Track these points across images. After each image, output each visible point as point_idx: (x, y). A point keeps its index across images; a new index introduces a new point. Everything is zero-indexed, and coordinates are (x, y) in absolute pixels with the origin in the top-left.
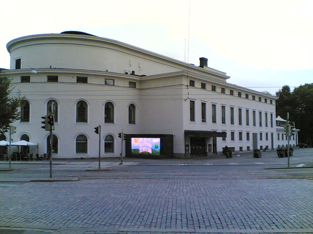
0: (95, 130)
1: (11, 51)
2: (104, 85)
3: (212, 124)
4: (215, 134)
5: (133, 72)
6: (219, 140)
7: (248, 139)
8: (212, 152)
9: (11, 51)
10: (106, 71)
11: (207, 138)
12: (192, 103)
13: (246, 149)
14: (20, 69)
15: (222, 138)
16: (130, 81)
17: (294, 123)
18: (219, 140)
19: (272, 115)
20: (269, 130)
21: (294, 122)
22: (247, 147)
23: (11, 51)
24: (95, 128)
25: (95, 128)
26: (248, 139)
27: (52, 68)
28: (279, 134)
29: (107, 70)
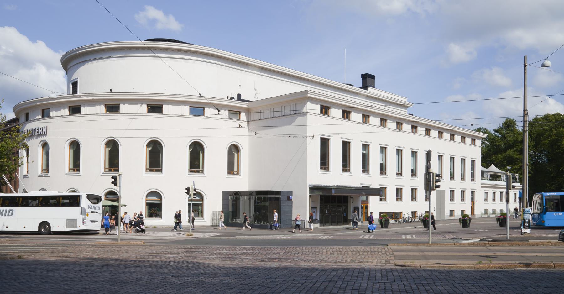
0: (186, 191)
1: (68, 68)
2: (227, 119)
3: (471, 183)
4: (368, 191)
5: (239, 96)
6: (374, 200)
7: (463, 199)
8: (90, 207)
9: (69, 68)
10: (199, 95)
11: (352, 198)
12: (325, 142)
13: (449, 214)
14: (77, 94)
15: (379, 196)
16: (148, 104)
17: (517, 175)
18: (374, 200)
19: (473, 162)
20: (468, 185)
21: (518, 174)
22: (450, 211)
23: (68, 68)
24: (186, 189)
25: (186, 189)
26: (463, 199)
27: (112, 92)
28: (486, 193)
29: (200, 94)
